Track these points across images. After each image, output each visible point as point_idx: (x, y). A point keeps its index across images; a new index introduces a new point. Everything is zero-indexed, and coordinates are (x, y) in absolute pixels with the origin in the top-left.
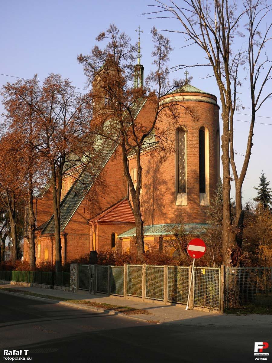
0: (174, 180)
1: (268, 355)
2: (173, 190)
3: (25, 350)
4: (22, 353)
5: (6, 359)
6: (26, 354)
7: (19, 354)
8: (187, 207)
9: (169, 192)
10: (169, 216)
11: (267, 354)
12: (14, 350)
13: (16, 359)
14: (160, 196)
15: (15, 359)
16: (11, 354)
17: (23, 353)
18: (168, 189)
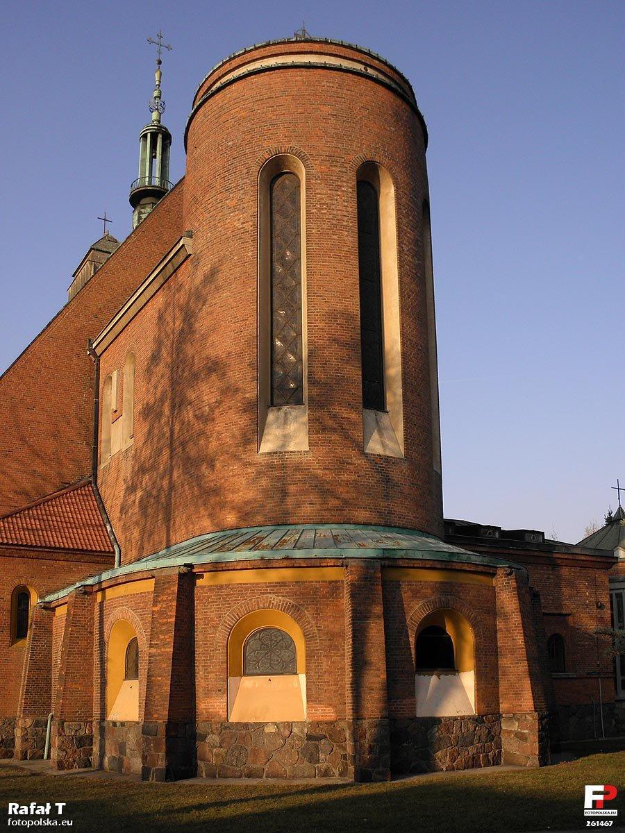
0: (251, 355)
1: (616, 815)
2: (251, 391)
3: (56, 804)
4: (50, 810)
5: (15, 823)
6: (60, 812)
7: (43, 813)
8: (309, 457)
9: (231, 403)
10: (230, 496)
11: (614, 813)
12: (32, 804)
13: (37, 823)
14: (198, 426)
15: (34, 823)
16: (26, 813)
17: (54, 809)
18: (229, 391)
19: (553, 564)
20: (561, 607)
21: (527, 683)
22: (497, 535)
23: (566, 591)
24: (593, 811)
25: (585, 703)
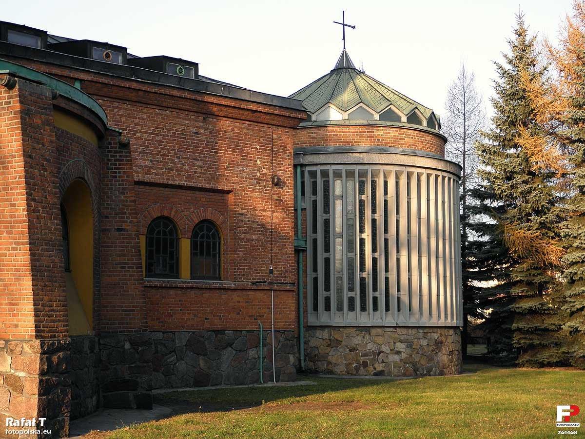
1: (579, 426)
3: (40, 419)
6: (42, 424)
11: (578, 425)
12: (23, 419)
16: (18, 425)
19: (205, 113)
20: (216, 178)
21: (27, 283)
22: (120, 61)
23: (226, 155)
24: (562, 423)
25: (249, 328)
